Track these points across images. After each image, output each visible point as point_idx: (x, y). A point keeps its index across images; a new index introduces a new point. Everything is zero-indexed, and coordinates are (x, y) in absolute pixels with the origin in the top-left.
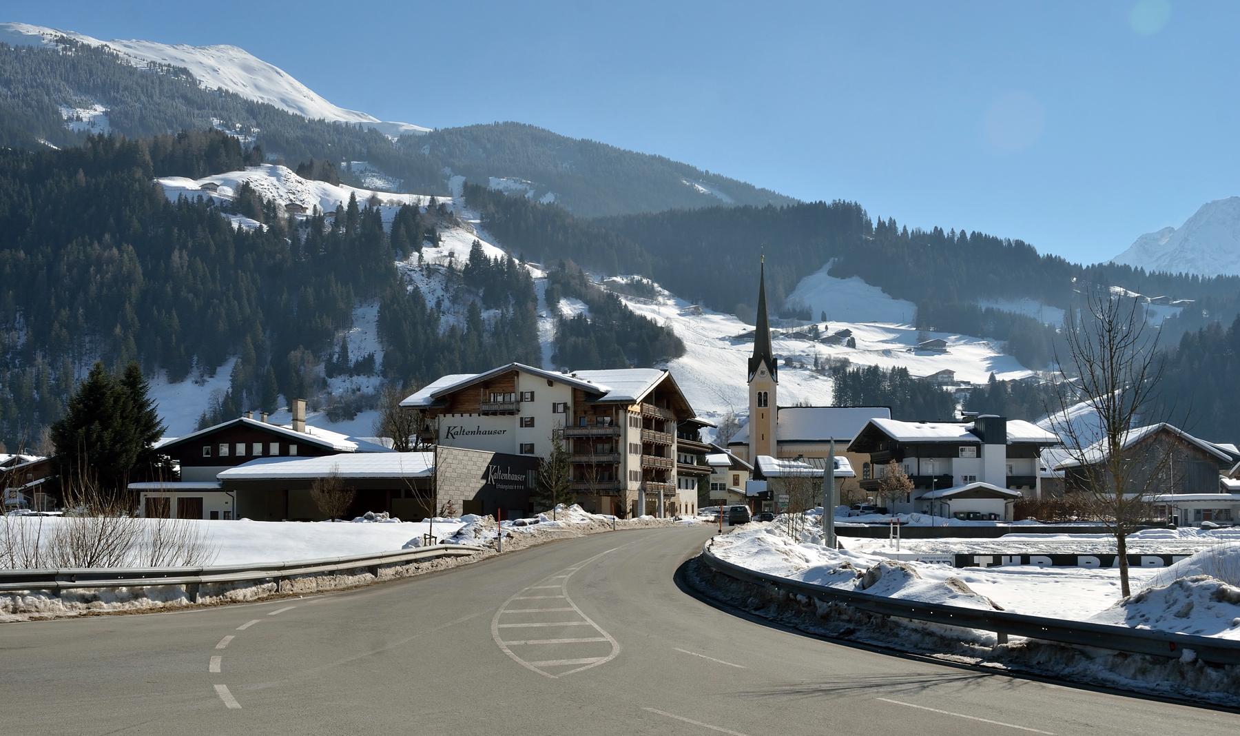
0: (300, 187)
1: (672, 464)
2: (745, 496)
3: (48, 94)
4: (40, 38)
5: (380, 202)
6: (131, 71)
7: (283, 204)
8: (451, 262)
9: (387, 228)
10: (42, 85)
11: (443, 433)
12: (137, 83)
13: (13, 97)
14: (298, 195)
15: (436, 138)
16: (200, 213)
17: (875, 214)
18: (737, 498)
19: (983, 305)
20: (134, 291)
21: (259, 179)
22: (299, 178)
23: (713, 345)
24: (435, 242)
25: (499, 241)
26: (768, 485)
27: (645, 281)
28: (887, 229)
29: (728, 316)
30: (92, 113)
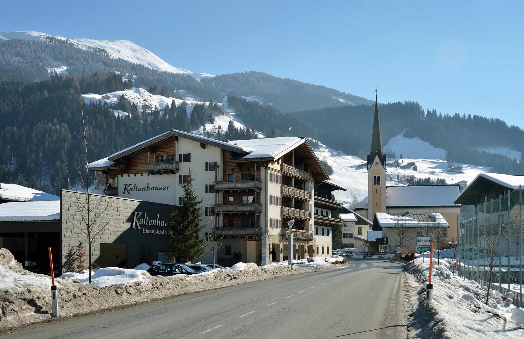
0: (150, 98)
1: (310, 216)
2: (367, 241)
3: (42, 62)
4: (39, 37)
5: (187, 104)
6: (79, 51)
7: (141, 105)
8: (219, 131)
9: (189, 115)
10: (39, 57)
11: (121, 189)
12: (82, 56)
13: (26, 63)
14: (149, 102)
15: (218, 79)
16: (100, 110)
17: (426, 107)
18: (361, 243)
19: (480, 150)
20: (66, 145)
21: (130, 94)
22: (149, 94)
23: (347, 170)
24: (212, 121)
25: (243, 121)
26: (383, 234)
27: (314, 140)
28: (432, 114)
29: (354, 157)
30: (61, 70)
